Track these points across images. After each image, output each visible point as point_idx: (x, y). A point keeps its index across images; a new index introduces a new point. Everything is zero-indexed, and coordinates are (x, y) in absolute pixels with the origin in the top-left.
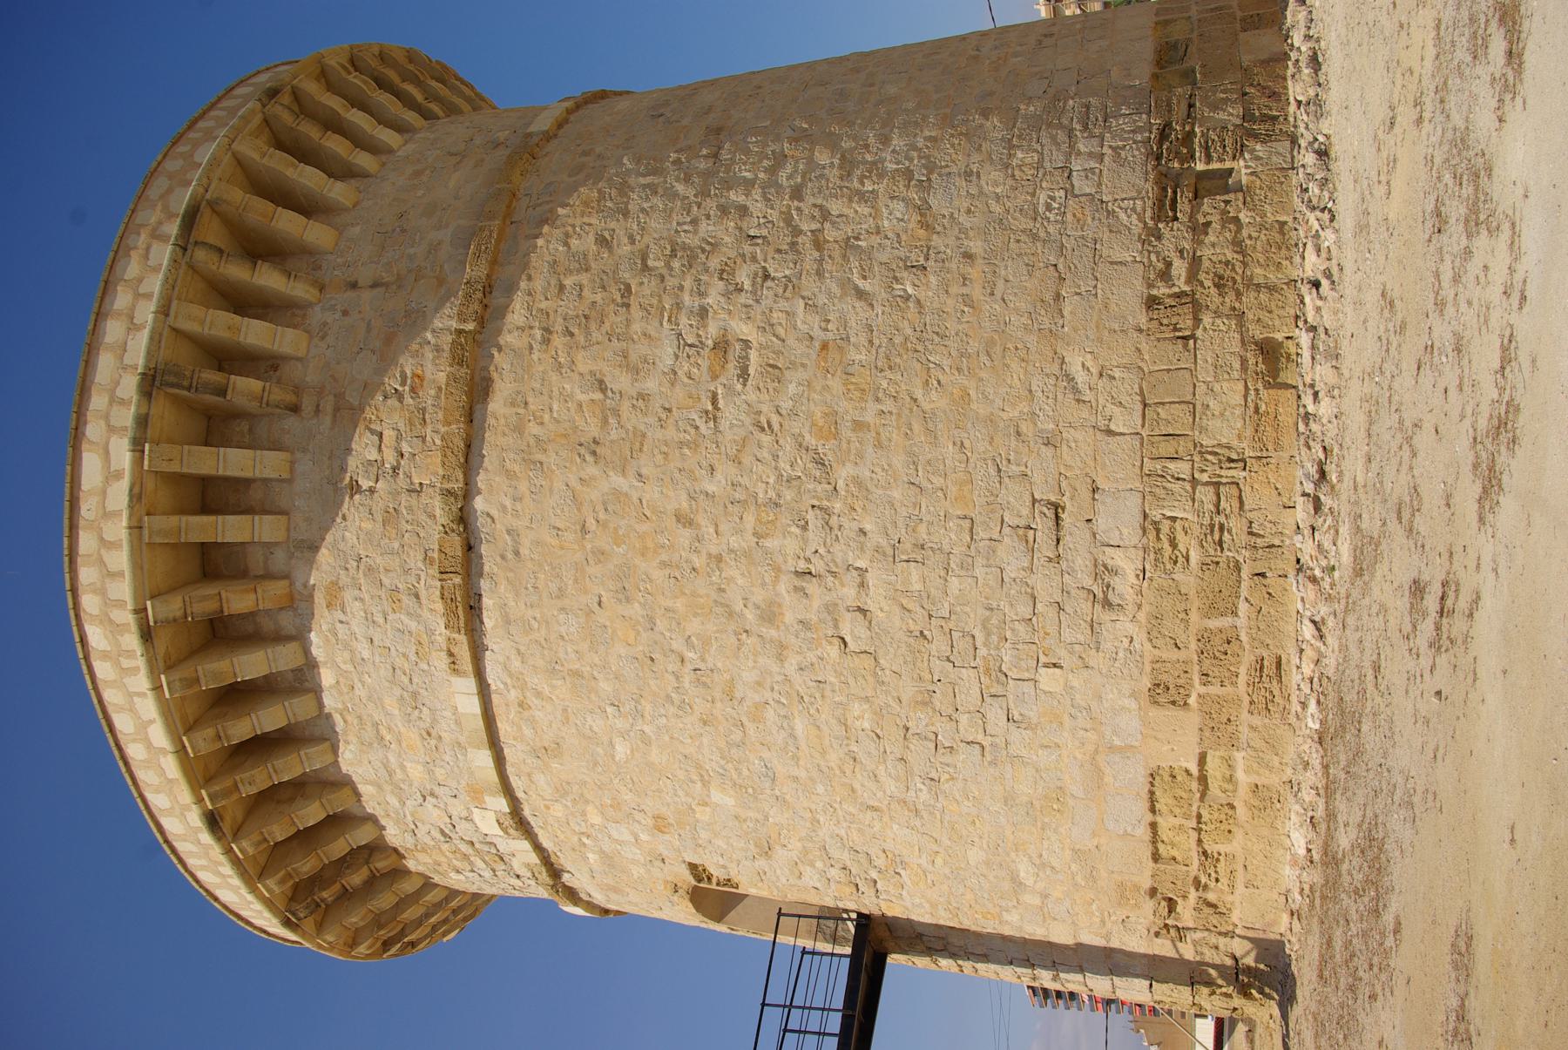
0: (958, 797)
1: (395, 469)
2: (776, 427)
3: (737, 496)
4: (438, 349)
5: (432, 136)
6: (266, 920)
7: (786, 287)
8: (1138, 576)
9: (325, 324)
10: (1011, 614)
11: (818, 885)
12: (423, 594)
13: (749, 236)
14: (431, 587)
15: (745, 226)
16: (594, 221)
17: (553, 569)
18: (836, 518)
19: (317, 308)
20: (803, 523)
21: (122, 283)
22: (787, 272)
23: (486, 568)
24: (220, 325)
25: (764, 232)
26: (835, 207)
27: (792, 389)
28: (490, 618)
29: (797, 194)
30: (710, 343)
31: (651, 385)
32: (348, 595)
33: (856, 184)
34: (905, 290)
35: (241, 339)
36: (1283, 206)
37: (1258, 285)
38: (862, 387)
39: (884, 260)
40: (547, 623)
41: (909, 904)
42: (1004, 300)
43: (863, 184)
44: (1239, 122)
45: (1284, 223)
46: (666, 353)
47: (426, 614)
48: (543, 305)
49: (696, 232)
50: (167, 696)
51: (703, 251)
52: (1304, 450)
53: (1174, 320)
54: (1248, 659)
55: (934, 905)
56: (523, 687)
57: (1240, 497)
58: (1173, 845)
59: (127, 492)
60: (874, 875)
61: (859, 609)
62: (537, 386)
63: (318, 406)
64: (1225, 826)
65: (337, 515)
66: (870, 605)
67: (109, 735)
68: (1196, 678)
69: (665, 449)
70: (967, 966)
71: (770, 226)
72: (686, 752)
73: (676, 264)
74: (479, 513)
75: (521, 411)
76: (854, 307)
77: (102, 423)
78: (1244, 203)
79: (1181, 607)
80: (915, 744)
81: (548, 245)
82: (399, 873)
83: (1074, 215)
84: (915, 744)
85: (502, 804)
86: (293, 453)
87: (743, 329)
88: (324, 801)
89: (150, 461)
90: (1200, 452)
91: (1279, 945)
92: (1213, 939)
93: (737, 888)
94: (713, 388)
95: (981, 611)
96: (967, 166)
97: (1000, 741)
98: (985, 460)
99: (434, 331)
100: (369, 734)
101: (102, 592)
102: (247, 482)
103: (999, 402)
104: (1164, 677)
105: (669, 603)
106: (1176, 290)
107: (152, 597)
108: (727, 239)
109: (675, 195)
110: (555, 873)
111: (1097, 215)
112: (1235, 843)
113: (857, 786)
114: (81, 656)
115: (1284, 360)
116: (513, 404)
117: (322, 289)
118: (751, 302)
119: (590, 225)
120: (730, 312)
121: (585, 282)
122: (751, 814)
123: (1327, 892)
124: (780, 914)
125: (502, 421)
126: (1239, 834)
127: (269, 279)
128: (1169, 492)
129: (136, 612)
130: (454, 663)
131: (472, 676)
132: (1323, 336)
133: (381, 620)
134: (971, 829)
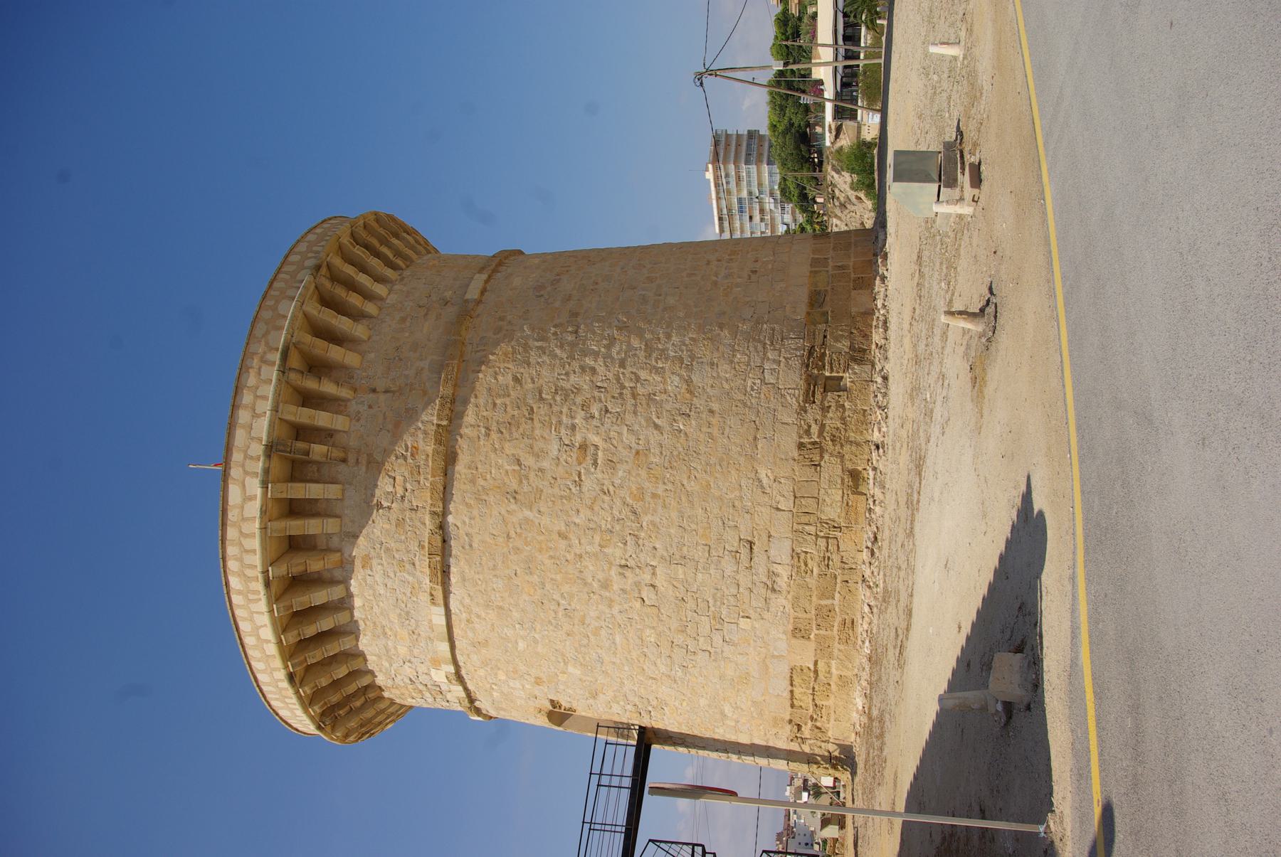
0: (696, 675)
1: (403, 497)
2: (612, 493)
3: (591, 526)
4: (425, 433)
5: (405, 289)
6: (310, 728)
7: (617, 418)
8: (788, 578)
9: (359, 412)
10: (727, 592)
11: (620, 712)
12: (417, 563)
13: (597, 386)
14: (422, 560)
15: (594, 379)
16: (510, 366)
17: (491, 555)
18: (641, 540)
19: (354, 402)
20: (624, 541)
21: (246, 388)
22: (618, 410)
23: (454, 552)
24: (305, 416)
25: (605, 385)
26: (643, 374)
27: (621, 473)
28: (454, 577)
29: (622, 364)
30: (577, 444)
31: (545, 464)
32: (375, 562)
33: (654, 363)
34: (679, 427)
35: (316, 423)
36: (865, 401)
37: (851, 442)
38: (657, 476)
39: (668, 409)
40: (486, 582)
41: (667, 723)
42: (728, 437)
43: (657, 363)
44: (847, 350)
45: (865, 411)
46: (554, 448)
47: (418, 574)
48: (485, 414)
49: (568, 380)
50: (276, 615)
51: (573, 392)
52: (868, 526)
53: (811, 457)
54: (838, 619)
55: (680, 724)
56: (470, 613)
57: (838, 545)
58: (801, 701)
59: (259, 510)
60: (650, 709)
61: (652, 585)
62: (483, 459)
63: (358, 460)
64: (826, 693)
65: (369, 519)
66: (657, 583)
67: (236, 632)
68: (814, 627)
69: (553, 499)
70: (693, 751)
71: (608, 382)
72: (557, 648)
73: (558, 398)
74: (450, 524)
75: (474, 472)
76: (653, 434)
77: (241, 469)
78: (847, 398)
79: (808, 594)
80: (676, 650)
81: (485, 378)
82: (381, 698)
83: (765, 395)
84: (676, 650)
85: (451, 669)
86: (343, 485)
87: (594, 439)
88: (349, 665)
89: (272, 493)
90: (820, 522)
91: (851, 747)
92: (819, 743)
93: (575, 712)
94: (579, 469)
95: (713, 591)
96: (711, 359)
97: (719, 651)
98: (717, 518)
99: (422, 422)
100: (379, 630)
101: (241, 560)
102: (316, 500)
103: (725, 490)
104: (799, 626)
105: (553, 576)
106: (813, 440)
107: (271, 565)
108: (585, 387)
109: (555, 356)
110: (471, 700)
111: (776, 396)
112: (830, 701)
113: (645, 667)
114: (225, 592)
115: (861, 480)
116: (469, 468)
117: (355, 390)
118: (598, 425)
119: (509, 368)
120: (588, 429)
121: (508, 403)
122: (588, 678)
123: (868, 729)
124: (598, 726)
125: (463, 476)
126: (832, 697)
127: (328, 387)
128: (805, 540)
129: (263, 572)
130: (433, 599)
131: (443, 606)
132: (879, 474)
133: (392, 576)
134: (702, 690)
